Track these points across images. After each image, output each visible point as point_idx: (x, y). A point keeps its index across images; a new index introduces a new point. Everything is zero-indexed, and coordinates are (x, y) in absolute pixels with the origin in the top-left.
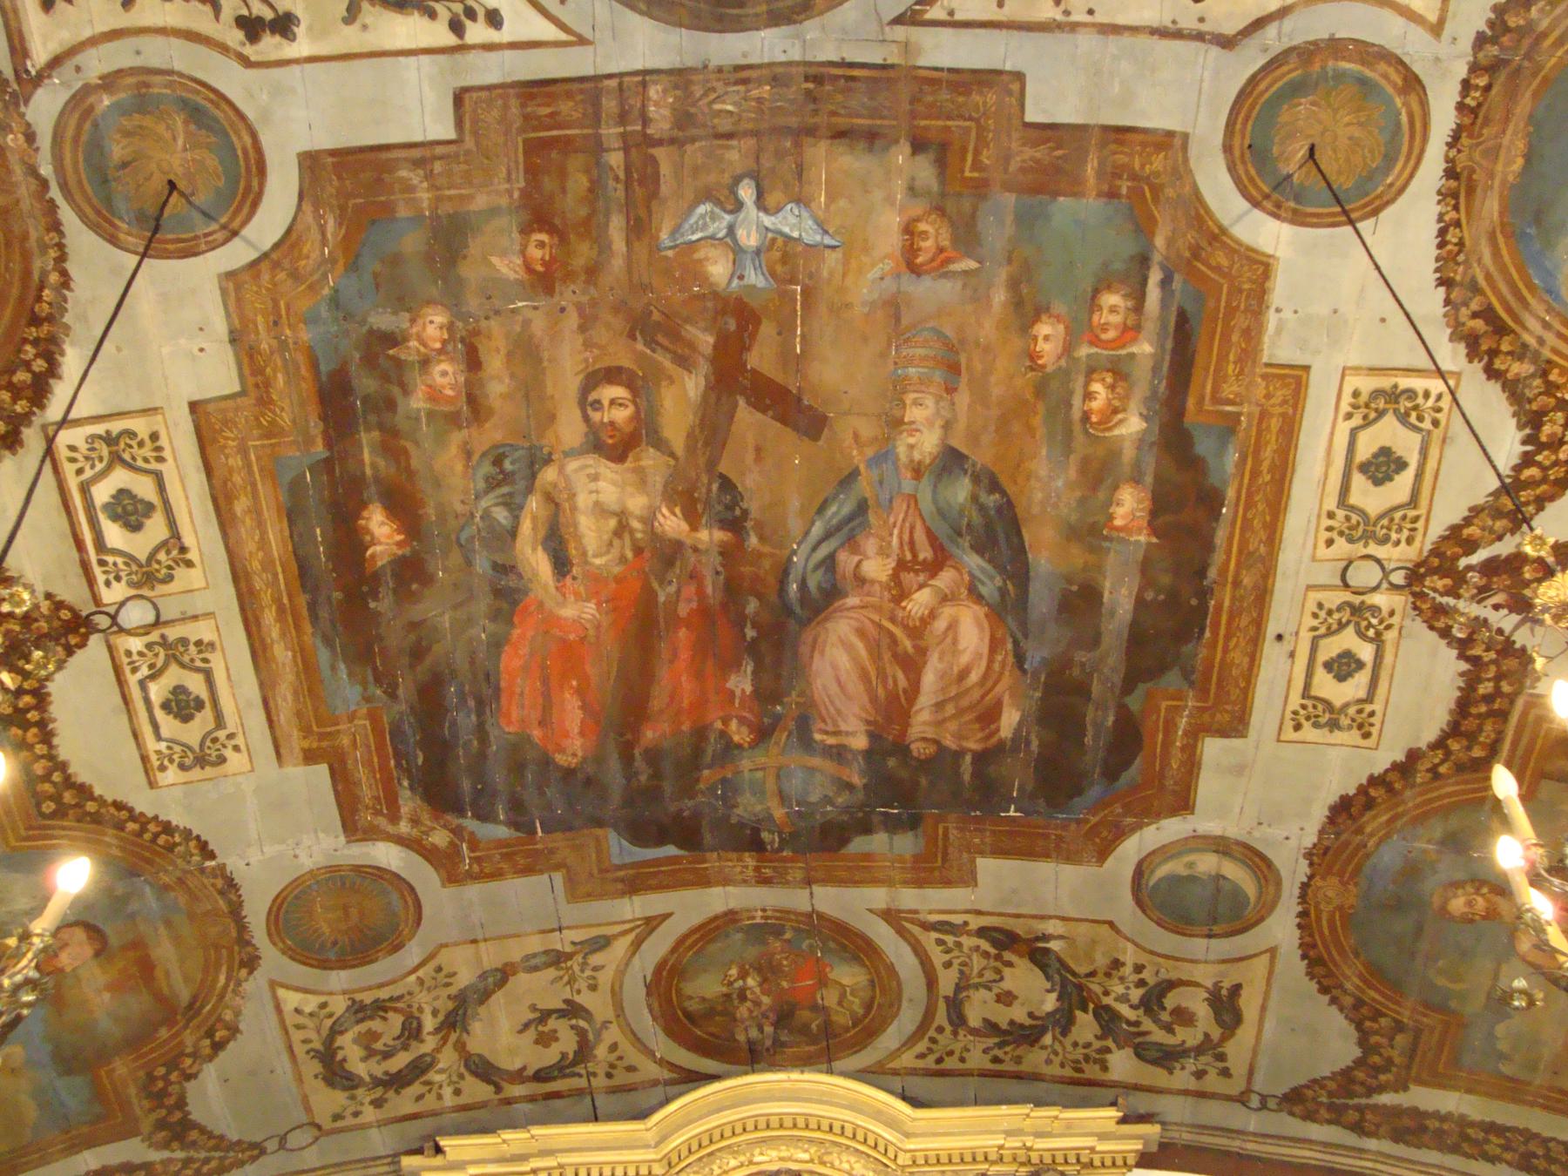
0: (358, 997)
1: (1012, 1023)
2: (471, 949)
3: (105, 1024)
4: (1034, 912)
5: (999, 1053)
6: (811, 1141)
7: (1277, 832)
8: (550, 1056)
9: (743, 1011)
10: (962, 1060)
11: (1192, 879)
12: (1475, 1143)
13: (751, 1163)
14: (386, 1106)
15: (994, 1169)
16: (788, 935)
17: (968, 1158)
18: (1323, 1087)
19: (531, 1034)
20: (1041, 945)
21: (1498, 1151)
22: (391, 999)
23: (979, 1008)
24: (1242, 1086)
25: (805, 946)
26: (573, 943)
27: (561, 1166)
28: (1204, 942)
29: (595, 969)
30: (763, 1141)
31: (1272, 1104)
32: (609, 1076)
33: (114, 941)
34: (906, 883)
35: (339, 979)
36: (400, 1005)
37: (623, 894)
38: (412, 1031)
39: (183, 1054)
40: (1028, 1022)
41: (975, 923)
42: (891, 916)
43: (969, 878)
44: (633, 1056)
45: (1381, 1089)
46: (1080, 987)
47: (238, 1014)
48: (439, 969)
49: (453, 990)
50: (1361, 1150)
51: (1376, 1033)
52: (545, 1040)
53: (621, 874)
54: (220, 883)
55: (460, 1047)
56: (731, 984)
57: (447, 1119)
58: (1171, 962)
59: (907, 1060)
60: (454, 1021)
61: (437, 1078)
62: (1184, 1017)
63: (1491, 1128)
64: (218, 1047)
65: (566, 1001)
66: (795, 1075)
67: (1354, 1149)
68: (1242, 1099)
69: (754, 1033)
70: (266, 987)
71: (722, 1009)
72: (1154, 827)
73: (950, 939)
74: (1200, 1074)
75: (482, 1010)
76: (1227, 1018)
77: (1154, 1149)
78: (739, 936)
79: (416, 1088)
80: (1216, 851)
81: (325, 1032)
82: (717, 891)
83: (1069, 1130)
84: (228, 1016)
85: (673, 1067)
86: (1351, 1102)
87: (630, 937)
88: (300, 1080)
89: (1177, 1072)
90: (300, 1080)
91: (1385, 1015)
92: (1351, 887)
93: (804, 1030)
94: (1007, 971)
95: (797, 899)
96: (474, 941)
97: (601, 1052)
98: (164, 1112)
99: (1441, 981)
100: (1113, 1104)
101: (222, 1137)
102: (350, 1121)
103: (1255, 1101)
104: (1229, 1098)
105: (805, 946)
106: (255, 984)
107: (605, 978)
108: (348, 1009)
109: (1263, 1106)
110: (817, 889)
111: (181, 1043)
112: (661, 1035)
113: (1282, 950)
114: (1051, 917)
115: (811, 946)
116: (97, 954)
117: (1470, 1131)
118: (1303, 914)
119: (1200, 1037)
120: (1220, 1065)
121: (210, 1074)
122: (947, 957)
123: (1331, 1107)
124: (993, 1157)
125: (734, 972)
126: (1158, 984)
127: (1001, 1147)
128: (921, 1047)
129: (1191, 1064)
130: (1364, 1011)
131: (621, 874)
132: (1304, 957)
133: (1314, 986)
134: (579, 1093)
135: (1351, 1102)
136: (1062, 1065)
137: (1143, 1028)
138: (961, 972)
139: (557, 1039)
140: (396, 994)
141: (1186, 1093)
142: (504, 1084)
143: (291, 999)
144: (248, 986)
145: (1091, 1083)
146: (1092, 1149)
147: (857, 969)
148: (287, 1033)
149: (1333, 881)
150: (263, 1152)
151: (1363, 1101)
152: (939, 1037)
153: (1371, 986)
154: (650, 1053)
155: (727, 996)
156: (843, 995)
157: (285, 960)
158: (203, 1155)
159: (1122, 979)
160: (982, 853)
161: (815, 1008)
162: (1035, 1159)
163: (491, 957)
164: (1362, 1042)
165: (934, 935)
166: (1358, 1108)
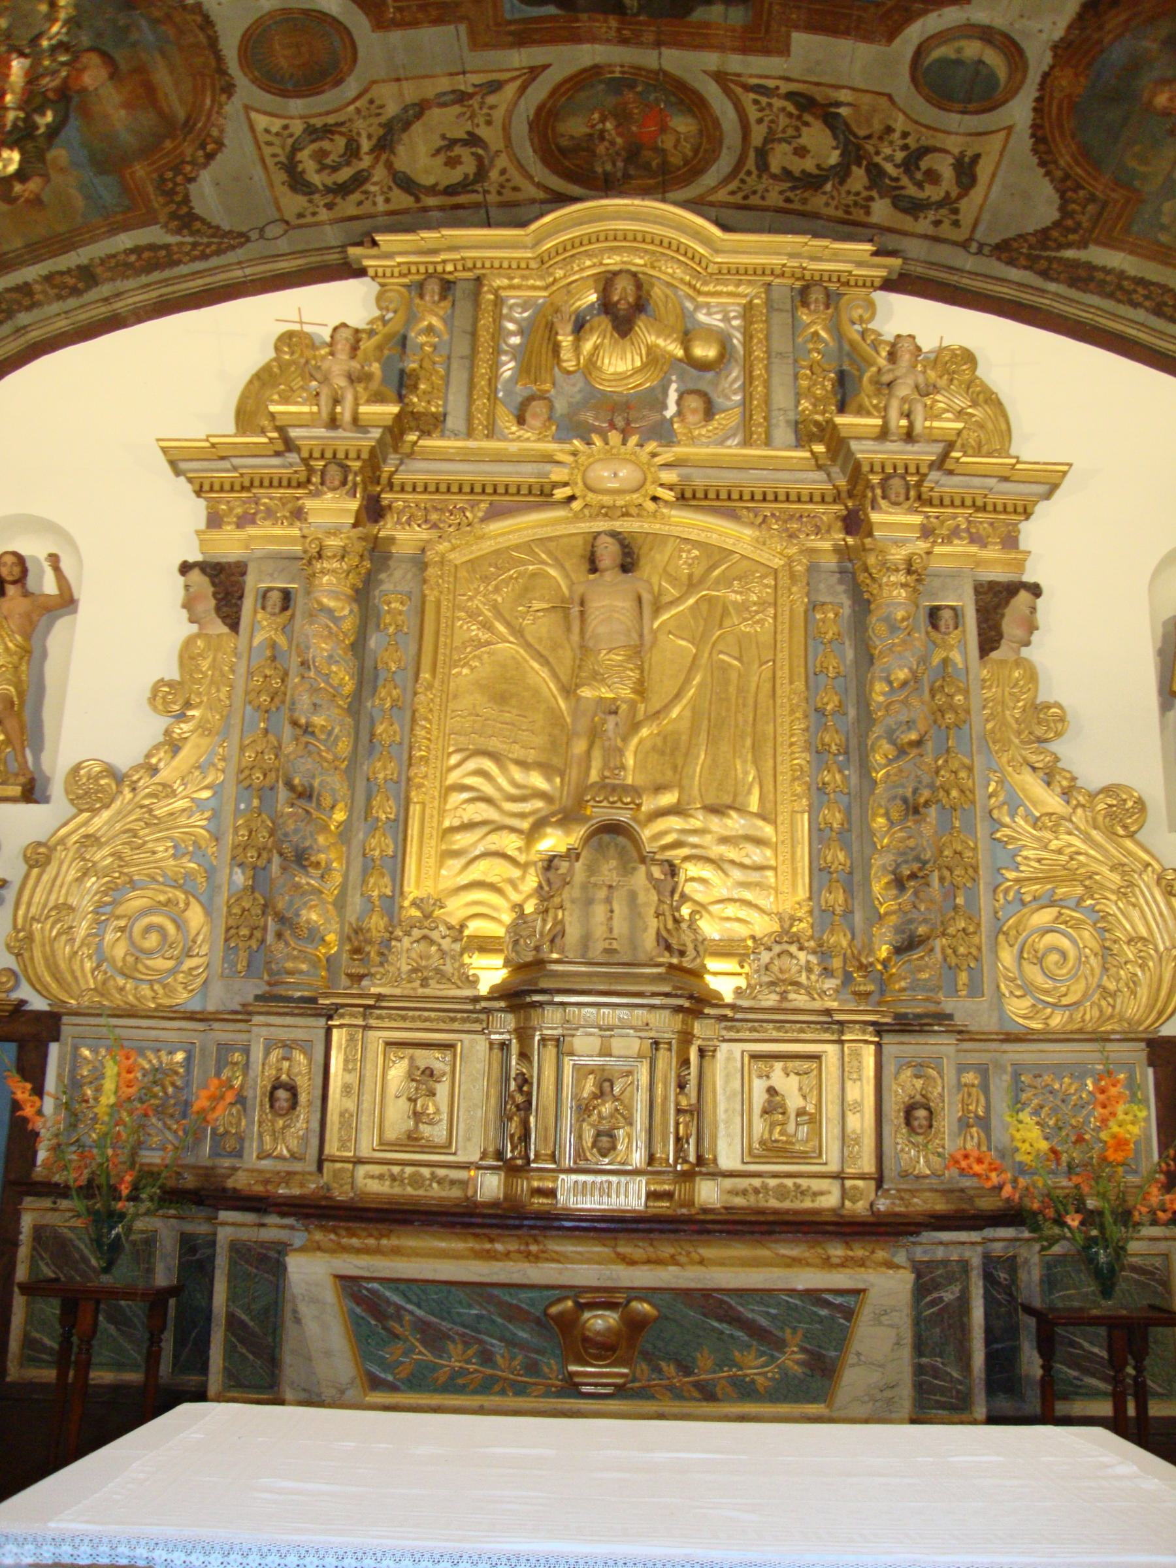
0: (313, 121)
1: (803, 172)
2: (395, 85)
3: (127, 138)
4: (833, 82)
5: (789, 194)
6: (646, 251)
7: (1035, 25)
8: (455, 176)
9: (601, 149)
10: (763, 198)
11: (958, 62)
12: (1128, 293)
13: (601, 264)
14: (336, 208)
15: (778, 281)
16: (639, 89)
17: (759, 272)
18: (1026, 241)
19: (441, 159)
20: (833, 110)
21: (1141, 299)
22: (337, 124)
23: (780, 158)
24: (967, 236)
25: (652, 98)
26: (475, 86)
27: (463, 259)
28: (958, 117)
29: (491, 108)
30: (611, 249)
31: (986, 250)
32: (499, 193)
33: (124, 67)
34: (734, 50)
35: (297, 106)
36: (343, 129)
37: (512, 46)
38: (352, 151)
39: (184, 162)
40: (816, 172)
41: (785, 87)
42: (720, 77)
43: (784, 50)
44: (518, 179)
45: (1069, 245)
46: (859, 148)
47: (222, 131)
48: (371, 102)
49: (383, 119)
50: (1043, 291)
51: (1074, 202)
52: (452, 163)
53: (513, 28)
54: (199, 19)
55: (389, 166)
56: (593, 126)
57: (382, 220)
58: (931, 132)
59: (722, 195)
60: (385, 144)
61: (373, 189)
62: (933, 177)
63: (1141, 282)
64: (210, 157)
65: (469, 133)
66: (637, 202)
67: (1037, 289)
68: (964, 245)
69: (609, 167)
70: (242, 112)
71: (586, 147)
72: (935, 14)
73: (764, 100)
74: (937, 223)
75: (405, 136)
76: (965, 180)
77: (895, 276)
78: (602, 87)
79: (356, 196)
80: (981, 39)
81: (288, 149)
82: (586, 47)
83: (835, 257)
84: (215, 132)
85: (546, 189)
86: (1045, 254)
87: (518, 83)
88: (271, 185)
89: (921, 220)
90: (271, 185)
91: (1083, 188)
92: (1082, 79)
93: (647, 167)
94: (804, 130)
95: (648, 58)
96: (398, 80)
97: (494, 174)
98: (173, 207)
99: (1133, 164)
100: (871, 241)
101: (218, 228)
102: (309, 219)
103: (974, 247)
104: (955, 243)
105: (652, 98)
106: (233, 107)
107: (498, 115)
108: (305, 131)
109: (979, 252)
110: (666, 51)
111: (182, 154)
112: (539, 165)
113: (1018, 128)
114: (843, 87)
115: (656, 99)
116: (112, 77)
117: (1125, 283)
118: (1039, 100)
119: (942, 194)
120: (954, 217)
121: (205, 176)
122: (760, 115)
123: (1028, 257)
124: (777, 272)
125: (596, 116)
126: (918, 149)
127: (784, 265)
128: (733, 186)
129: (931, 215)
130: (1069, 183)
131: (513, 28)
132: (1033, 136)
133: (1035, 160)
134: (477, 206)
135: (1045, 254)
136: (837, 208)
137: (901, 183)
138: (769, 128)
139: (461, 163)
140: (342, 119)
141: (925, 237)
142: (422, 196)
143: (261, 121)
144: (228, 109)
145: (855, 224)
146: (850, 272)
147: (690, 120)
148: (259, 148)
149: (1069, 72)
150: (248, 240)
151: (1053, 254)
152: (748, 179)
153: (1078, 164)
154: (530, 178)
155: (591, 136)
156: (678, 141)
157: (254, 89)
158: (205, 240)
159: (891, 143)
160: (797, 28)
161: (656, 149)
162: (808, 277)
163: (411, 92)
164: (1062, 208)
165: (752, 96)
166: (1048, 259)
